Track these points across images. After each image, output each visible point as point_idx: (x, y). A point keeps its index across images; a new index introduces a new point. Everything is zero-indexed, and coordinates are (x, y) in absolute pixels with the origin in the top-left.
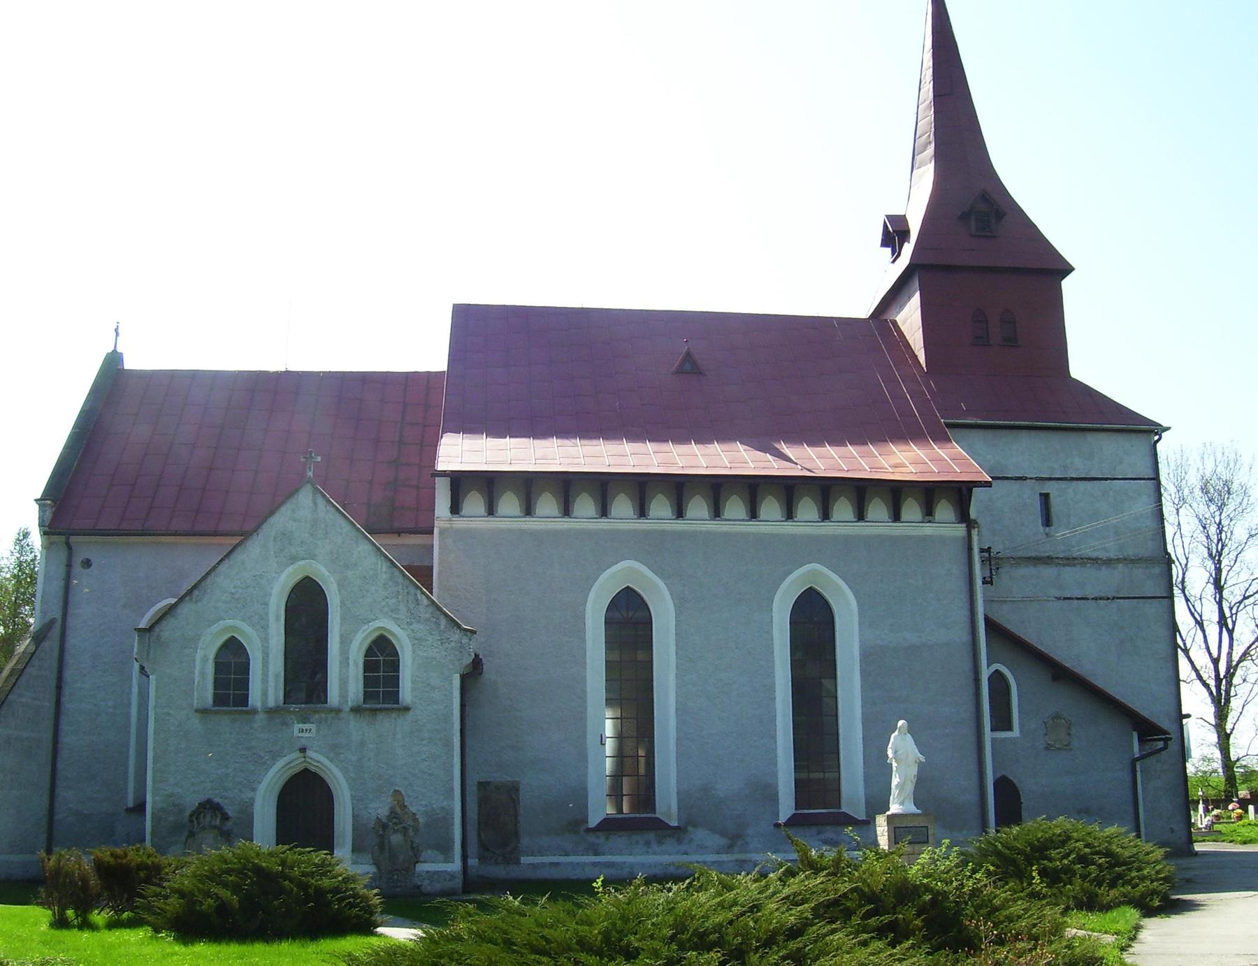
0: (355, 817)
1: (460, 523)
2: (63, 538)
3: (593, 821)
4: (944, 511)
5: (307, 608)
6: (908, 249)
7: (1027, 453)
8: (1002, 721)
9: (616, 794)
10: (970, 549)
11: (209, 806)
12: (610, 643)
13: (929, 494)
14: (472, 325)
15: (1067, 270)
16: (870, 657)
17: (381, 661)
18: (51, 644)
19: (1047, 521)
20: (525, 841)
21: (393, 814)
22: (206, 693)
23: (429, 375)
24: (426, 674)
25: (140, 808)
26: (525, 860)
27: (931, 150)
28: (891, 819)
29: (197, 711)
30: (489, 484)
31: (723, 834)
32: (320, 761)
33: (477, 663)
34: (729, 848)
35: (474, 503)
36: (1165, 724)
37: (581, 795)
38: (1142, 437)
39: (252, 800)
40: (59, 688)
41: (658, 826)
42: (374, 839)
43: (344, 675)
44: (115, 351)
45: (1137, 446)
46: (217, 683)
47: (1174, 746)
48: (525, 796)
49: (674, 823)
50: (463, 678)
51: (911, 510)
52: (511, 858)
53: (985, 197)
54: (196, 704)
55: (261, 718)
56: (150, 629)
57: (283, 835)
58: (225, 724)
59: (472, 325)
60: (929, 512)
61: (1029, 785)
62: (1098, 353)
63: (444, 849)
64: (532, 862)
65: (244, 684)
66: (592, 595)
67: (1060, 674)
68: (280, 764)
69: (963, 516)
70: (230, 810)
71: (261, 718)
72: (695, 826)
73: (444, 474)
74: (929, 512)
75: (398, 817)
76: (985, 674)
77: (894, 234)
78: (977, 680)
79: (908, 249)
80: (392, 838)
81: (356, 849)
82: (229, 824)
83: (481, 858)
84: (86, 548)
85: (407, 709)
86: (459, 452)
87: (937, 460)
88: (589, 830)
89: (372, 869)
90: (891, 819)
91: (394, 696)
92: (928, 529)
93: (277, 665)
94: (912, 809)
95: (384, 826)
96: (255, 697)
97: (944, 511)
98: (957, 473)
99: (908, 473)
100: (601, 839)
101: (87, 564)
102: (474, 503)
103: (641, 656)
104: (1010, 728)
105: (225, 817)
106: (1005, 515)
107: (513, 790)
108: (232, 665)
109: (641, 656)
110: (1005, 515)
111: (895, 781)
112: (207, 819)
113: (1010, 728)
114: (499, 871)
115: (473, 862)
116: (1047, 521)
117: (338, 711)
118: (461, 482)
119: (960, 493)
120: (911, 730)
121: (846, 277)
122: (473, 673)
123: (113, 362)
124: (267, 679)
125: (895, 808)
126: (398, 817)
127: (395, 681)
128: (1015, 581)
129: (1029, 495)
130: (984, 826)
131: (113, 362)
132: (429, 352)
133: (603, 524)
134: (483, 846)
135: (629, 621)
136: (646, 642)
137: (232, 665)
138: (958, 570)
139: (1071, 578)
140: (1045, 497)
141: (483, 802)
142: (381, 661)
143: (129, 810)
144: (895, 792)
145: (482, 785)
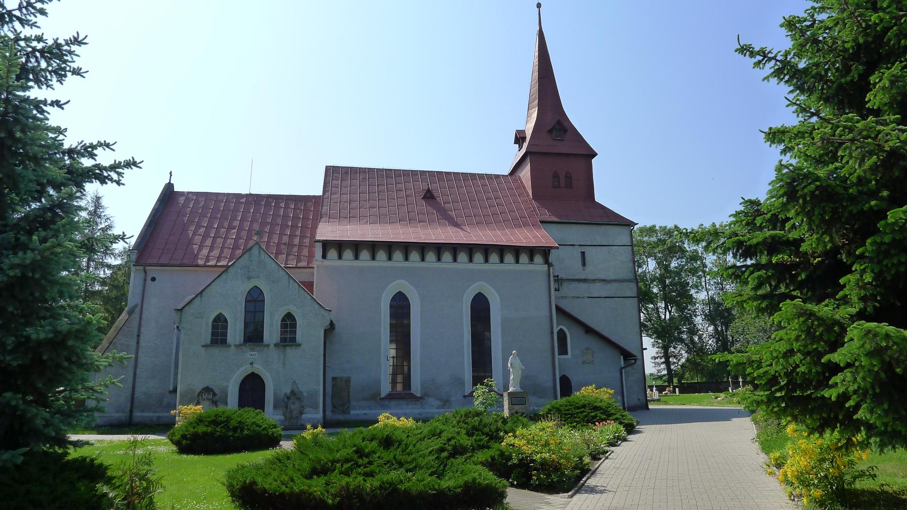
0: (275, 394)
1: (326, 263)
2: (142, 268)
3: (383, 395)
4: (538, 259)
5: (255, 300)
6: (525, 145)
7: (576, 234)
8: (563, 350)
9: (394, 383)
10: (549, 275)
11: (207, 390)
12: (392, 316)
13: (532, 252)
14: (333, 174)
15: (595, 155)
16: (504, 321)
17: (289, 322)
18: (136, 315)
19: (584, 264)
20: (353, 403)
21: (293, 392)
22: (207, 337)
23: (314, 197)
24: (309, 333)
25: (175, 391)
26: (352, 412)
27: (536, 102)
28: (510, 394)
29: (203, 346)
30: (340, 246)
31: (441, 400)
32: (259, 369)
33: (332, 324)
34: (443, 407)
35: (332, 253)
36: (634, 352)
37: (378, 382)
38: (625, 227)
39: (227, 387)
40: (139, 336)
41: (413, 397)
42: (282, 403)
43: (272, 331)
44: (170, 183)
45: (624, 231)
46: (213, 334)
47: (639, 362)
48: (353, 384)
49: (419, 395)
50: (326, 331)
51: (524, 258)
52: (346, 411)
53: (559, 123)
54: (203, 343)
55: (233, 348)
56: (181, 310)
57: (241, 404)
58: (216, 351)
59: (333, 174)
60: (531, 259)
61: (574, 379)
62: (606, 193)
63: (315, 407)
64: (356, 413)
65: (225, 334)
66: (384, 295)
67: (589, 330)
68: (241, 369)
69: (547, 262)
70: (216, 391)
71: (233, 348)
72: (428, 396)
73: (319, 241)
74: (531, 259)
75: (294, 395)
76: (556, 331)
77: (519, 139)
78: (552, 333)
79: (525, 145)
80: (292, 402)
81: (276, 407)
82: (217, 398)
83: (333, 411)
84: (153, 271)
85: (299, 345)
86: (327, 231)
87: (535, 237)
88: (381, 399)
89: (282, 418)
90: (510, 394)
91: (293, 340)
92: (531, 267)
93: (240, 326)
94: (519, 390)
95: (288, 398)
96: (230, 339)
97: (538, 259)
98: (543, 243)
99: (523, 242)
100: (387, 403)
101: (153, 279)
102: (332, 253)
103: (405, 322)
104: (566, 353)
105: (215, 394)
106: (566, 262)
107: (348, 381)
108: (220, 323)
109: (405, 322)
110: (566, 262)
111: (512, 377)
112: (205, 396)
113: (566, 353)
114: (340, 417)
115: (328, 413)
116: (584, 264)
117: (268, 346)
118: (327, 245)
119: (545, 252)
120: (518, 355)
121: (498, 157)
122: (330, 329)
123: (169, 187)
124: (235, 332)
125: (511, 390)
126: (294, 395)
127: (225, 334)
128: (568, 290)
129: (577, 251)
130: (556, 398)
131: (169, 187)
132: (314, 187)
133: (390, 264)
134: (334, 406)
135: (400, 307)
136: (407, 315)
137: (220, 323)
138: (544, 285)
139: (598, 290)
140: (583, 253)
141: (334, 386)
142: (289, 322)
143: (170, 392)
144: (511, 382)
145: (334, 379)
